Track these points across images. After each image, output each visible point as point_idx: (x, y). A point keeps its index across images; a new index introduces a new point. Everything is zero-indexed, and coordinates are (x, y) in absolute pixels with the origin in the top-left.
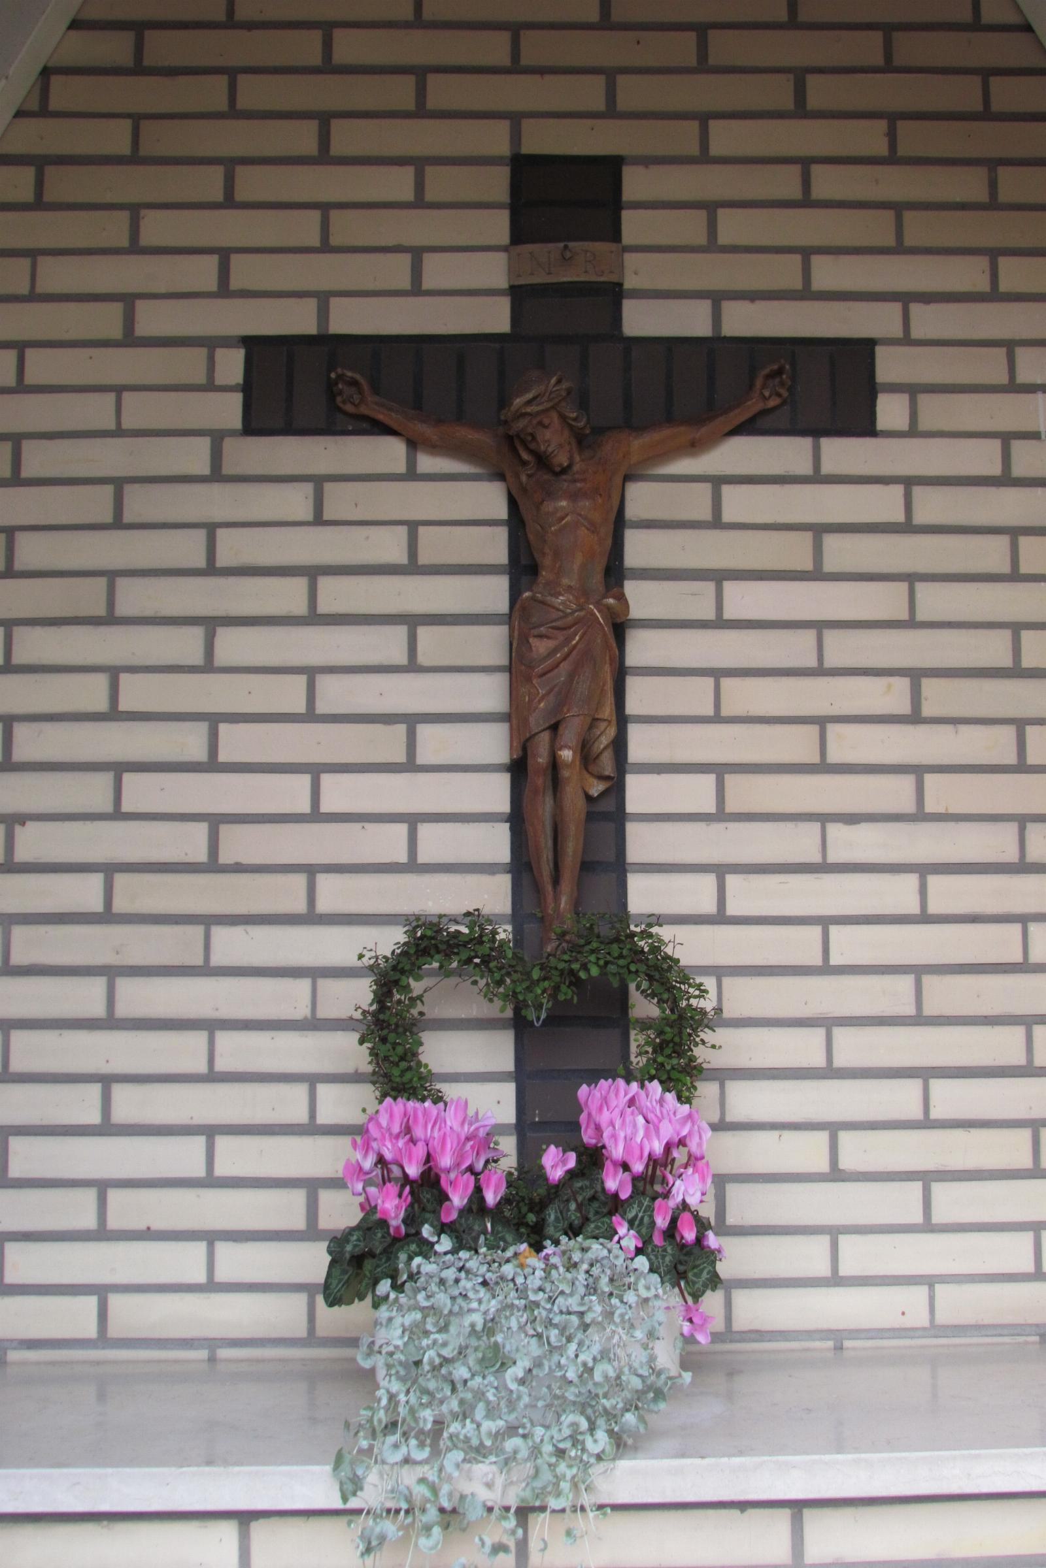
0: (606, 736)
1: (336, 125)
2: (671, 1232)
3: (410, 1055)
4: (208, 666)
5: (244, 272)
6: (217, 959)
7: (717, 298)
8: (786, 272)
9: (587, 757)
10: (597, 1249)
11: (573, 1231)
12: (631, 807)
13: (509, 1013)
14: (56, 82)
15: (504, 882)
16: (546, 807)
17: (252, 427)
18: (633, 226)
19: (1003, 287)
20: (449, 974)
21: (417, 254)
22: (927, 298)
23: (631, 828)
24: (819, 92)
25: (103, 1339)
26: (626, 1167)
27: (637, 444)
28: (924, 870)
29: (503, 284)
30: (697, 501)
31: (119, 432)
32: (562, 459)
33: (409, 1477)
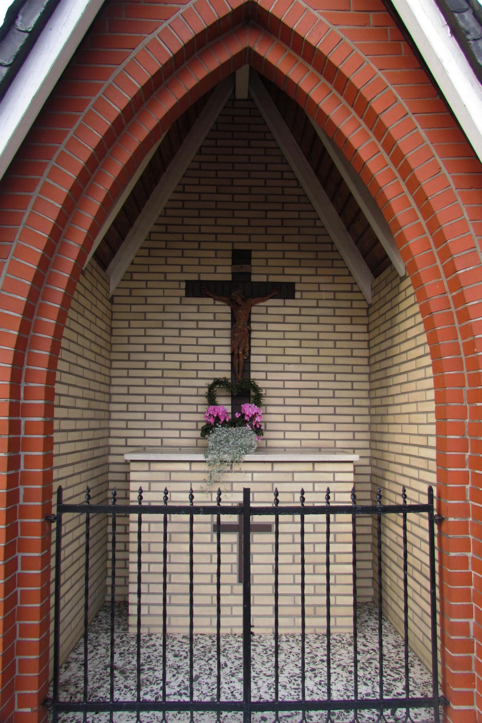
0: (247, 349)
1: (201, 243)
2: (255, 426)
3: (214, 400)
4: (180, 336)
5: (185, 269)
6: (181, 385)
7: (268, 275)
8: (280, 270)
9: (244, 352)
10: (244, 428)
11: (240, 426)
12: (251, 361)
13: (230, 394)
14: (152, 234)
15: (230, 373)
16: (237, 361)
17: (187, 296)
18: (253, 262)
19: (318, 273)
20: (221, 387)
21: (216, 266)
22: (304, 275)
23: (251, 365)
24: (286, 239)
25: (162, 446)
26: (248, 416)
27: (253, 300)
28: (301, 373)
29: (230, 272)
30: (263, 310)
31: (164, 296)
32: (240, 303)
33: (215, 456)
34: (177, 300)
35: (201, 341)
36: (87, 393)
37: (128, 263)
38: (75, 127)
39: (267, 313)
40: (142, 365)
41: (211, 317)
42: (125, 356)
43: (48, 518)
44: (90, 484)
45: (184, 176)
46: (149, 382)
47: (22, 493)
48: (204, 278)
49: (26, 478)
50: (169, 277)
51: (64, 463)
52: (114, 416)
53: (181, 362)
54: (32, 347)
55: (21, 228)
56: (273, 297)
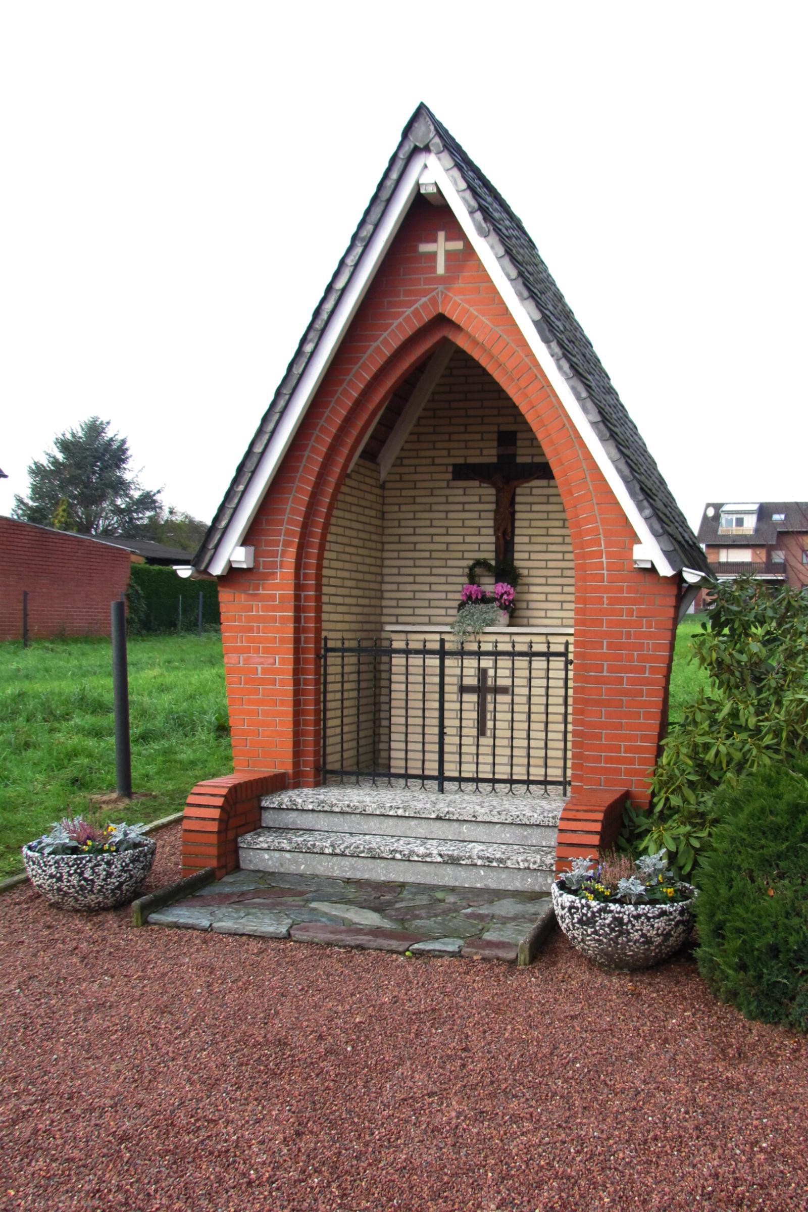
5: (453, 452)
17: (454, 479)
18: (519, 443)
21: (481, 449)
30: (528, 491)
31: (432, 480)
34: (444, 484)
35: (467, 523)
36: (355, 575)
37: (399, 448)
38: (330, 408)
39: (531, 494)
40: (411, 547)
41: (476, 499)
42: (396, 539)
43: (318, 657)
44: (347, 635)
45: (451, 360)
46: (418, 563)
47: (303, 639)
48: (470, 460)
49: (305, 630)
50: (437, 461)
51: (333, 628)
52: (386, 595)
53: (448, 544)
54: (309, 537)
55: (299, 475)
56: (538, 478)
